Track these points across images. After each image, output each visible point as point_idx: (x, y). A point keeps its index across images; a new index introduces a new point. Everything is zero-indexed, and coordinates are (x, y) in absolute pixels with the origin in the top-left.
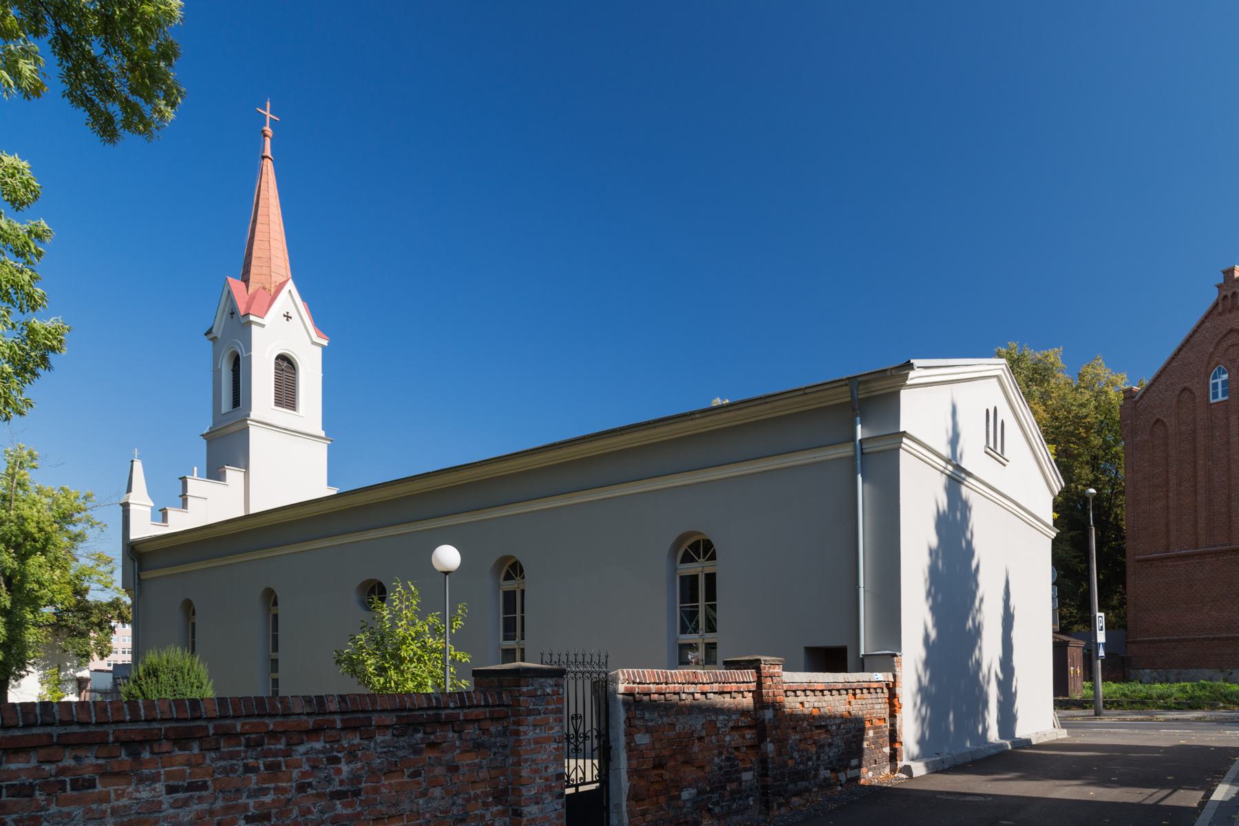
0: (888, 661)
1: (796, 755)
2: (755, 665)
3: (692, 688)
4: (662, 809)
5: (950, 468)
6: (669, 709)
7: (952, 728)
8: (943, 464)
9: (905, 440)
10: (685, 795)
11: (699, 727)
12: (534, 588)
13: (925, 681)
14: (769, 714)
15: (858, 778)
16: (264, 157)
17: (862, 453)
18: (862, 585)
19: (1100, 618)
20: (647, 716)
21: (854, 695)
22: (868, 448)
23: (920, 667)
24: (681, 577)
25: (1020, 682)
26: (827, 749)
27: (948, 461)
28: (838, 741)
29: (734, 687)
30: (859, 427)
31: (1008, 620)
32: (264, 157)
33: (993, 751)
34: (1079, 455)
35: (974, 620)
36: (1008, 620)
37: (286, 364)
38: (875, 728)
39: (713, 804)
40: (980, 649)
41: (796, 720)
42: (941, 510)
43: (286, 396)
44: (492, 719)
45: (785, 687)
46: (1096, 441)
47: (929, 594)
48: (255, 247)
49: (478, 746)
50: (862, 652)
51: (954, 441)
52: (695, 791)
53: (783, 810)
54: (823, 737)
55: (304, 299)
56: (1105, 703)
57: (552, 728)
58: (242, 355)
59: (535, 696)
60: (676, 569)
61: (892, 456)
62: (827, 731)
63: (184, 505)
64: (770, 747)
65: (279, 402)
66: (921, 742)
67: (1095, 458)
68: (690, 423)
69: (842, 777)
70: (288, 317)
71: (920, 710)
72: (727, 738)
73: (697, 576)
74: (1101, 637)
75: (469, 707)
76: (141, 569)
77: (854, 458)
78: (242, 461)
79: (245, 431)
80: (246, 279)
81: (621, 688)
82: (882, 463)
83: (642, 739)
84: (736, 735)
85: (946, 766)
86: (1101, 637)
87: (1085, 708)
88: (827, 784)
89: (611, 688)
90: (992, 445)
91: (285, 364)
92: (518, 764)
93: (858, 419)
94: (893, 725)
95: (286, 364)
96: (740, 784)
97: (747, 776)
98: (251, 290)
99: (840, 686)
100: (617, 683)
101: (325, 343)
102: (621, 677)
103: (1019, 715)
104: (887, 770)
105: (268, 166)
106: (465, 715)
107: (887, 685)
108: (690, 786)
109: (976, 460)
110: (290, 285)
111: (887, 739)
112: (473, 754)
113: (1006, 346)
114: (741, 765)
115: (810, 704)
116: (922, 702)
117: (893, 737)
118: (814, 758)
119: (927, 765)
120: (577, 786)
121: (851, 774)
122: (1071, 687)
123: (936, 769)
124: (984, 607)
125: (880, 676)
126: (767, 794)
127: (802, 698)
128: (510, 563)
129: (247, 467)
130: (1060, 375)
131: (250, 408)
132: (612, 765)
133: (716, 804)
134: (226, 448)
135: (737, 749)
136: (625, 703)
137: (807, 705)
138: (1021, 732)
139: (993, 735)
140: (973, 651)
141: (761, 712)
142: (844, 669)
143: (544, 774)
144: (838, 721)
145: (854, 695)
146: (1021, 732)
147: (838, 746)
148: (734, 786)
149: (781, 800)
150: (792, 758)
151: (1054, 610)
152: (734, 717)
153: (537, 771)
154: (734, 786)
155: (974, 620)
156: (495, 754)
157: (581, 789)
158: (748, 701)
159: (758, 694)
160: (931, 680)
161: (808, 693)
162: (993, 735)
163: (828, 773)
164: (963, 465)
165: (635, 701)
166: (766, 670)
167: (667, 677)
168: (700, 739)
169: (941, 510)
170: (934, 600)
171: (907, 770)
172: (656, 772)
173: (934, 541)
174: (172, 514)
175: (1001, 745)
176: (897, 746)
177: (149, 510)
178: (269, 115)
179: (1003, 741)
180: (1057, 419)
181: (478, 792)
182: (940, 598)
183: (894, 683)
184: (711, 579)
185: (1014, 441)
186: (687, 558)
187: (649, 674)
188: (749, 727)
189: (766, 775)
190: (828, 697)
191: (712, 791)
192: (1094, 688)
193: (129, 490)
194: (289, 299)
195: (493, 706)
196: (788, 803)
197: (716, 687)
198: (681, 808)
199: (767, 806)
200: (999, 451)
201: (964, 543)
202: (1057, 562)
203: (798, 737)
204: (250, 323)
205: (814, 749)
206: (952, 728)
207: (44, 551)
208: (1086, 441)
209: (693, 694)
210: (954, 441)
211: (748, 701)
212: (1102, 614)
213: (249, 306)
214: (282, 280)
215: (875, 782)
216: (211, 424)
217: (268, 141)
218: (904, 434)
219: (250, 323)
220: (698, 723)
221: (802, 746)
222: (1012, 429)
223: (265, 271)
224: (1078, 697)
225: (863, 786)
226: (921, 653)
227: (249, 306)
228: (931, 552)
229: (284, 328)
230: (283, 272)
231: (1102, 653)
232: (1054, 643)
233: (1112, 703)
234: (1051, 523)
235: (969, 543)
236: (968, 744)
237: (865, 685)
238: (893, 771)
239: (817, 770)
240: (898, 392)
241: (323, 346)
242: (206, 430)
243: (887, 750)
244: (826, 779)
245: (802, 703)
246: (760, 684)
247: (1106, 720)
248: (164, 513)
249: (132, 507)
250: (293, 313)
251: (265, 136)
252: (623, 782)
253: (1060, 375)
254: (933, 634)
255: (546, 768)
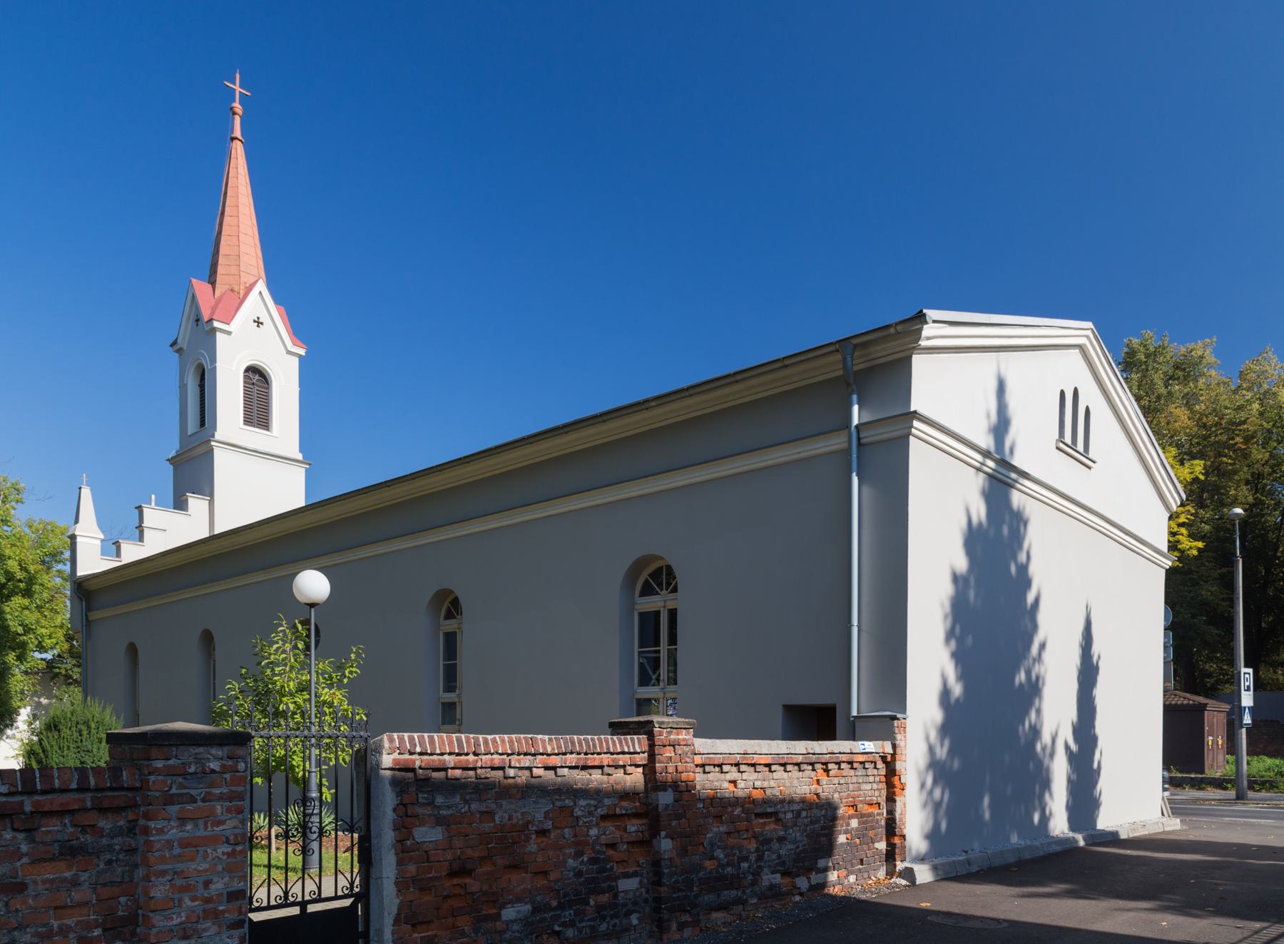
0: (885, 725)
1: (719, 854)
2: (646, 729)
3: (526, 761)
4: (463, 934)
5: (991, 464)
6: (483, 790)
7: (987, 815)
8: (979, 458)
9: (916, 423)
10: (509, 913)
11: (540, 816)
12: (474, 633)
13: (942, 753)
14: (665, 798)
15: (824, 885)
16: (233, 139)
17: (859, 444)
18: (855, 621)
19: (1247, 675)
20: (439, 800)
21: (827, 771)
22: (868, 436)
23: (933, 735)
24: (641, 614)
25: (1108, 754)
26: (776, 846)
27: (986, 454)
28: (795, 833)
29: (606, 759)
30: (856, 408)
31: (1088, 673)
32: (233, 139)
33: (1055, 848)
34: (1235, 472)
35: (1028, 673)
36: (1088, 673)
37: (257, 377)
38: (861, 816)
39: (564, 925)
40: (1039, 711)
41: (719, 806)
42: (975, 520)
43: (258, 411)
44: (102, 810)
45: (698, 760)
46: (1258, 454)
47: (950, 635)
48: (222, 243)
49: (70, 851)
50: (854, 713)
51: (1001, 427)
52: (528, 907)
53: (688, 932)
54: (771, 828)
55: (277, 301)
56: (1249, 781)
57: (221, 823)
58: (208, 367)
59: (184, 775)
60: (632, 605)
61: (901, 445)
62: (778, 820)
63: (141, 539)
64: (665, 845)
65: (248, 421)
66: (933, 836)
67: (1258, 477)
68: (646, 414)
69: (802, 883)
70: (258, 323)
71: (931, 793)
72: (594, 832)
73: (659, 612)
74: (1247, 700)
75: (44, 792)
76: (89, 609)
77: (848, 451)
78: (205, 486)
79: (210, 452)
80: (213, 283)
81: (387, 760)
82: (885, 459)
83: (428, 835)
84: (610, 827)
85: (974, 869)
86: (1247, 700)
87: (1226, 789)
88: (774, 893)
89: (371, 759)
90: (1068, 439)
91: (257, 377)
92: (147, 878)
93: (855, 397)
94: (891, 812)
95: (257, 377)
96: (615, 896)
97: (628, 885)
98: (218, 293)
99: (800, 759)
100: (381, 753)
101: (302, 352)
102: (386, 744)
103: (1103, 799)
104: (882, 873)
105: (238, 150)
106: (35, 804)
107: (884, 758)
108: (519, 900)
109: (1037, 458)
110: (261, 286)
111: (882, 831)
112: (62, 865)
113: (1140, 336)
114: (618, 869)
115: (748, 783)
116: (935, 782)
117: (891, 828)
118: (753, 857)
119: (935, 868)
120: (303, 905)
121: (815, 878)
122: (1207, 763)
123: (949, 874)
124: (1046, 656)
125: (869, 746)
126: (660, 909)
127: (733, 774)
128: (450, 599)
129: (211, 495)
130: (1213, 373)
131: (214, 428)
132: (374, 870)
133: (572, 924)
134: (191, 473)
135: (612, 846)
136: (395, 782)
137: (741, 784)
138: (1105, 821)
139: (1059, 825)
140: (1026, 713)
141: (653, 795)
142: (832, 737)
143: (201, 892)
144: (796, 807)
145: (827, 771)
146: (1105, 821)
147: (795, 841)
148: (604, 898)
149: (686, 918)
150: (712, 858)
151: (1166, 663)
152: (607, 802)
153: (186, 889)
154: (604, 898)
155: (1028, 673)
156: (109, 862)
157: (312, 908)
158: (636, 778)
159: (649, 769)
160: (952, 752)
161: (804, 767)
162: (1059, 825)
163: (777, 878)
164: (1016, 462)
165: (417, 780)
166: (662, 736)
167: (477, 744)
168: (542, 833)
169: (975, 520)
170: (960, 642)
171: (909, 874)
172: (455, 881)
173: (962, 563)
174: (125, 547)
175: (1067, 840)
176: (897, 840)
177: (99, 542)
178: (238, 89)
179: (1071, 834)
180: (1204, 426)
181: (69, 922)
182: (969, 640)
183: (894, 755)
184: (673, 614)
185: (1106, 435)
186: (647, 591)
187: (421, 740)
188: (636, 815)
189: (658, 883)
190: (779, 773)
191: (561, 907)
192: (1238, 763)
193: (77, 521)
194: (259, 302)
195: (98, 790)
196: (696, 922)
197: (572, 759)
198: (503, 932)
199: (661, 926)
200: (1080, 447)
201: (1013, 569)
202: (1174, 598)
203: (723, 829)
204: (214, 330)
205: (753, 846)
206: (987, 815)
207: (28, 593)
208: (1246, 455)
209: (530, 769)
210: (1001, 427)
211: (636, 778)
212: (1250, 670)
213: (214, 309)
214: (252, 280)
215: (857, 893)
216: (177, 446)
217: (237, 120)
218: (915, 415)
219: (214, 330)
220: (538, 812)
221: (732, 841)
222: (1103, 421)
223: (234, 270)
224: (1218, 775)
225: (834, 897)
226: (936, 715)
227: (214, 309)
228: (956, 578)
229: (255, 336)
230: (254, 271)
231: (1247, 719)
232: (1165, 705)
233: (1263, 783)
234: (1165, 549)
235: (1023, 569)
236: (1014, 839)
237: (844, 758)
238: (891, 873)
239: (757, 874)
240: (911, 357)
241: (300, 356)
242: (173, 454)
243: (882, 846)
244: (772, 887)
245: (734, 782)
246: (652, 756)
247: (1250, 807)
248: (117, 545)
249: (79, 539)
250: (264, 318)
251: (234, 114)
252: (389, 898)
253: (1213, 373)
254: (957, 690)
255: (207, 884)
